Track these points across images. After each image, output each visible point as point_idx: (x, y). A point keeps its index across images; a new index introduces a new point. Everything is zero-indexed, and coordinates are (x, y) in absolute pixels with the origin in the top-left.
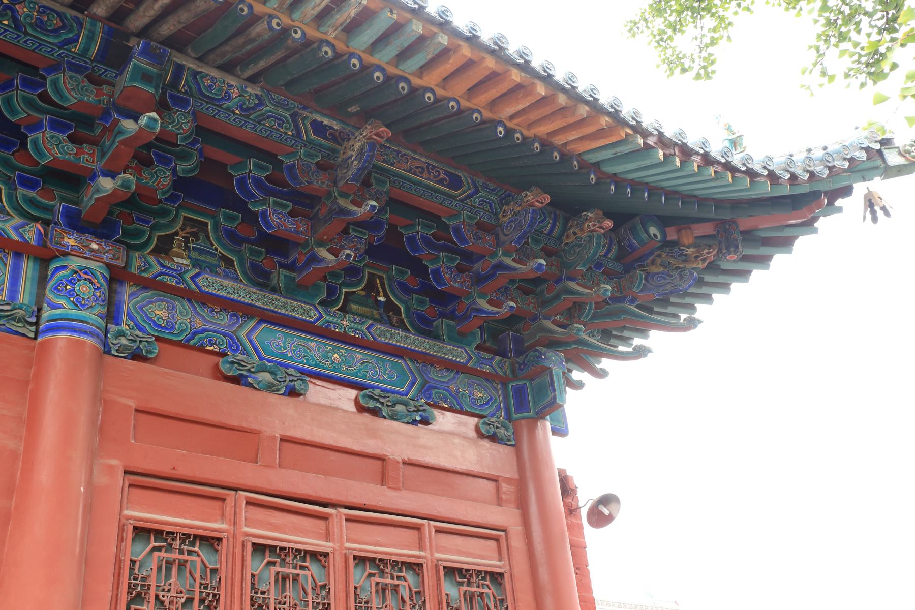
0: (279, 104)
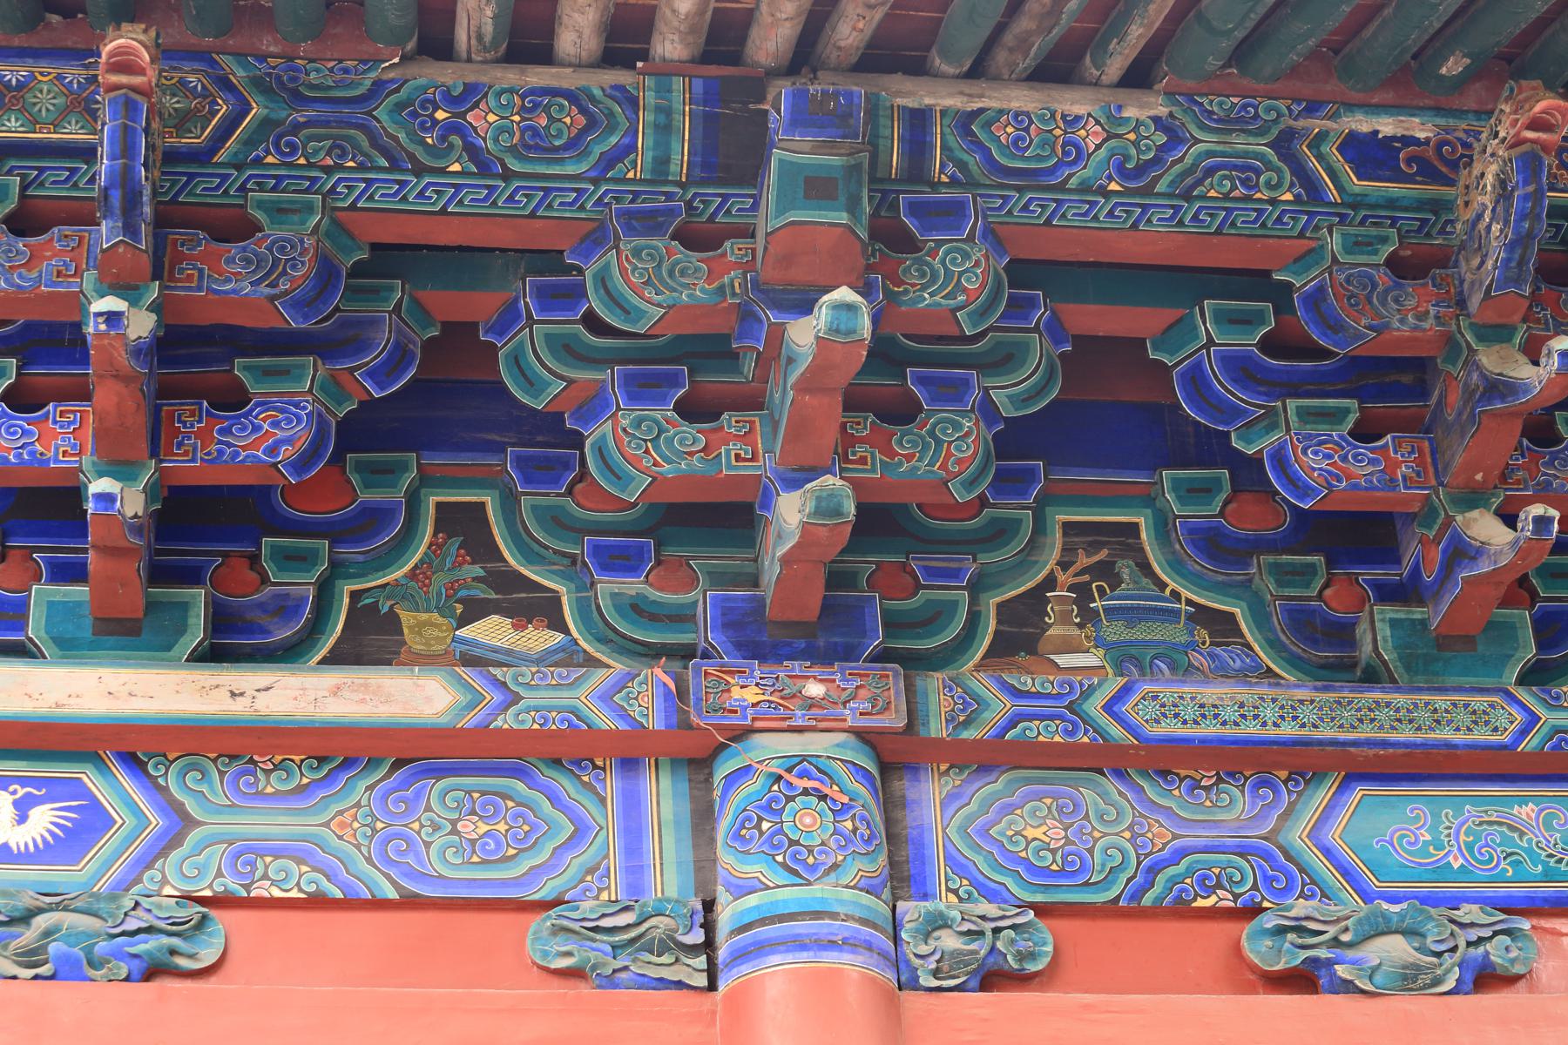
0: (1230, 124)
